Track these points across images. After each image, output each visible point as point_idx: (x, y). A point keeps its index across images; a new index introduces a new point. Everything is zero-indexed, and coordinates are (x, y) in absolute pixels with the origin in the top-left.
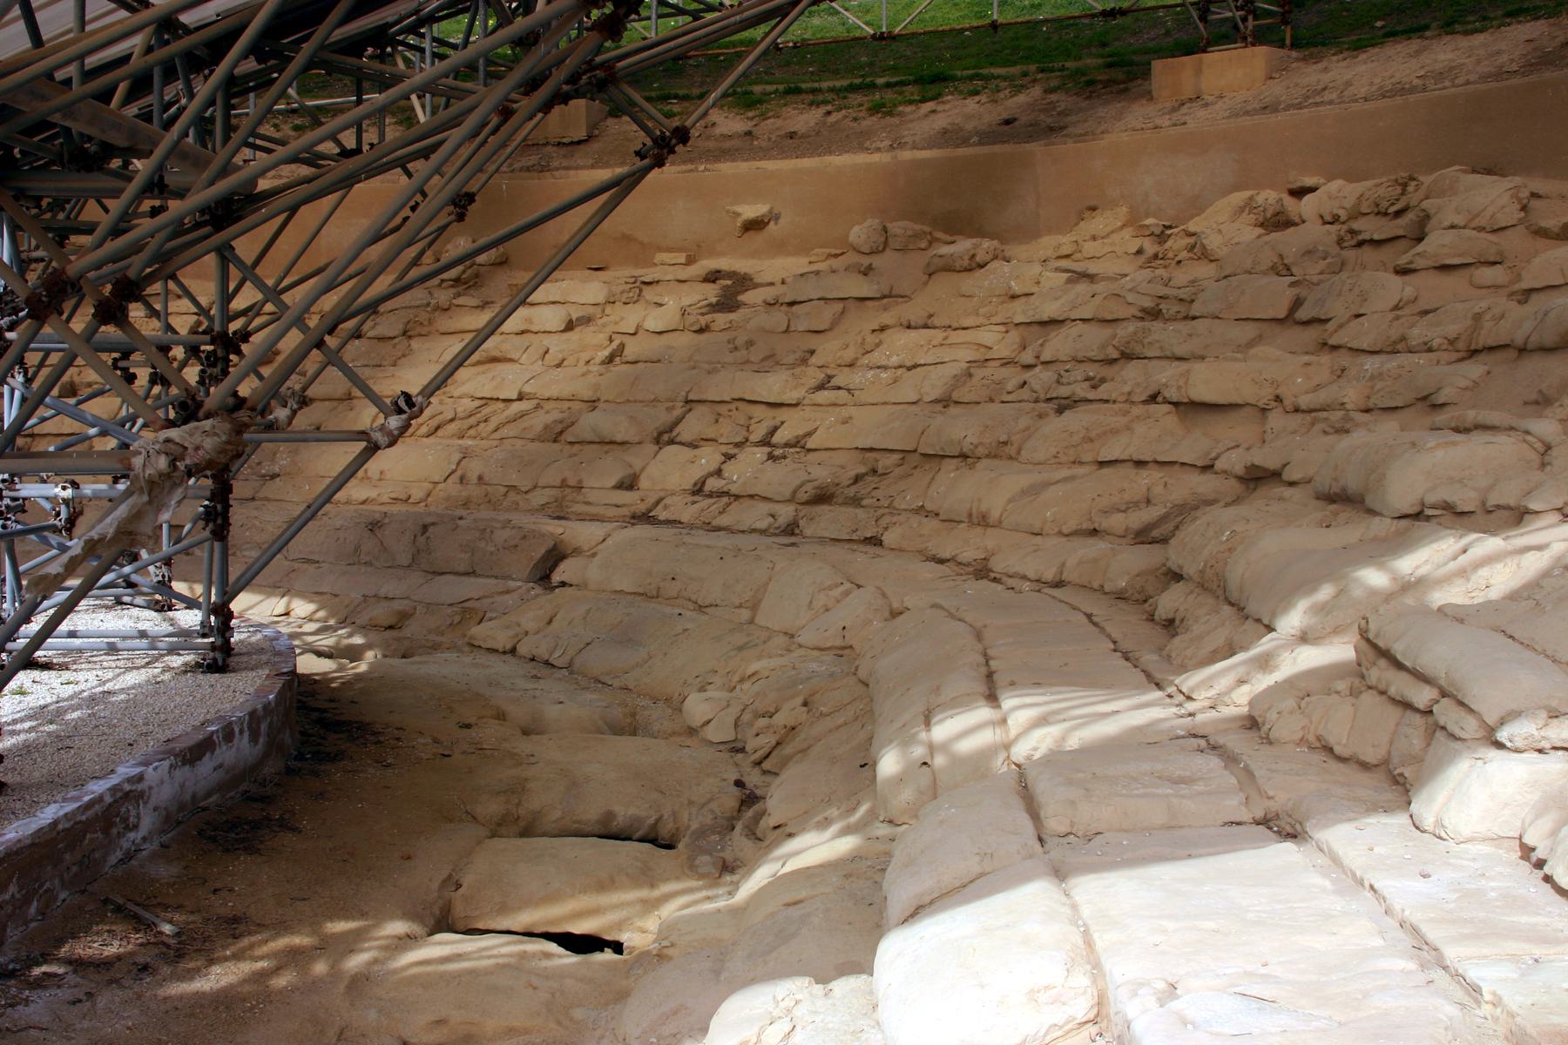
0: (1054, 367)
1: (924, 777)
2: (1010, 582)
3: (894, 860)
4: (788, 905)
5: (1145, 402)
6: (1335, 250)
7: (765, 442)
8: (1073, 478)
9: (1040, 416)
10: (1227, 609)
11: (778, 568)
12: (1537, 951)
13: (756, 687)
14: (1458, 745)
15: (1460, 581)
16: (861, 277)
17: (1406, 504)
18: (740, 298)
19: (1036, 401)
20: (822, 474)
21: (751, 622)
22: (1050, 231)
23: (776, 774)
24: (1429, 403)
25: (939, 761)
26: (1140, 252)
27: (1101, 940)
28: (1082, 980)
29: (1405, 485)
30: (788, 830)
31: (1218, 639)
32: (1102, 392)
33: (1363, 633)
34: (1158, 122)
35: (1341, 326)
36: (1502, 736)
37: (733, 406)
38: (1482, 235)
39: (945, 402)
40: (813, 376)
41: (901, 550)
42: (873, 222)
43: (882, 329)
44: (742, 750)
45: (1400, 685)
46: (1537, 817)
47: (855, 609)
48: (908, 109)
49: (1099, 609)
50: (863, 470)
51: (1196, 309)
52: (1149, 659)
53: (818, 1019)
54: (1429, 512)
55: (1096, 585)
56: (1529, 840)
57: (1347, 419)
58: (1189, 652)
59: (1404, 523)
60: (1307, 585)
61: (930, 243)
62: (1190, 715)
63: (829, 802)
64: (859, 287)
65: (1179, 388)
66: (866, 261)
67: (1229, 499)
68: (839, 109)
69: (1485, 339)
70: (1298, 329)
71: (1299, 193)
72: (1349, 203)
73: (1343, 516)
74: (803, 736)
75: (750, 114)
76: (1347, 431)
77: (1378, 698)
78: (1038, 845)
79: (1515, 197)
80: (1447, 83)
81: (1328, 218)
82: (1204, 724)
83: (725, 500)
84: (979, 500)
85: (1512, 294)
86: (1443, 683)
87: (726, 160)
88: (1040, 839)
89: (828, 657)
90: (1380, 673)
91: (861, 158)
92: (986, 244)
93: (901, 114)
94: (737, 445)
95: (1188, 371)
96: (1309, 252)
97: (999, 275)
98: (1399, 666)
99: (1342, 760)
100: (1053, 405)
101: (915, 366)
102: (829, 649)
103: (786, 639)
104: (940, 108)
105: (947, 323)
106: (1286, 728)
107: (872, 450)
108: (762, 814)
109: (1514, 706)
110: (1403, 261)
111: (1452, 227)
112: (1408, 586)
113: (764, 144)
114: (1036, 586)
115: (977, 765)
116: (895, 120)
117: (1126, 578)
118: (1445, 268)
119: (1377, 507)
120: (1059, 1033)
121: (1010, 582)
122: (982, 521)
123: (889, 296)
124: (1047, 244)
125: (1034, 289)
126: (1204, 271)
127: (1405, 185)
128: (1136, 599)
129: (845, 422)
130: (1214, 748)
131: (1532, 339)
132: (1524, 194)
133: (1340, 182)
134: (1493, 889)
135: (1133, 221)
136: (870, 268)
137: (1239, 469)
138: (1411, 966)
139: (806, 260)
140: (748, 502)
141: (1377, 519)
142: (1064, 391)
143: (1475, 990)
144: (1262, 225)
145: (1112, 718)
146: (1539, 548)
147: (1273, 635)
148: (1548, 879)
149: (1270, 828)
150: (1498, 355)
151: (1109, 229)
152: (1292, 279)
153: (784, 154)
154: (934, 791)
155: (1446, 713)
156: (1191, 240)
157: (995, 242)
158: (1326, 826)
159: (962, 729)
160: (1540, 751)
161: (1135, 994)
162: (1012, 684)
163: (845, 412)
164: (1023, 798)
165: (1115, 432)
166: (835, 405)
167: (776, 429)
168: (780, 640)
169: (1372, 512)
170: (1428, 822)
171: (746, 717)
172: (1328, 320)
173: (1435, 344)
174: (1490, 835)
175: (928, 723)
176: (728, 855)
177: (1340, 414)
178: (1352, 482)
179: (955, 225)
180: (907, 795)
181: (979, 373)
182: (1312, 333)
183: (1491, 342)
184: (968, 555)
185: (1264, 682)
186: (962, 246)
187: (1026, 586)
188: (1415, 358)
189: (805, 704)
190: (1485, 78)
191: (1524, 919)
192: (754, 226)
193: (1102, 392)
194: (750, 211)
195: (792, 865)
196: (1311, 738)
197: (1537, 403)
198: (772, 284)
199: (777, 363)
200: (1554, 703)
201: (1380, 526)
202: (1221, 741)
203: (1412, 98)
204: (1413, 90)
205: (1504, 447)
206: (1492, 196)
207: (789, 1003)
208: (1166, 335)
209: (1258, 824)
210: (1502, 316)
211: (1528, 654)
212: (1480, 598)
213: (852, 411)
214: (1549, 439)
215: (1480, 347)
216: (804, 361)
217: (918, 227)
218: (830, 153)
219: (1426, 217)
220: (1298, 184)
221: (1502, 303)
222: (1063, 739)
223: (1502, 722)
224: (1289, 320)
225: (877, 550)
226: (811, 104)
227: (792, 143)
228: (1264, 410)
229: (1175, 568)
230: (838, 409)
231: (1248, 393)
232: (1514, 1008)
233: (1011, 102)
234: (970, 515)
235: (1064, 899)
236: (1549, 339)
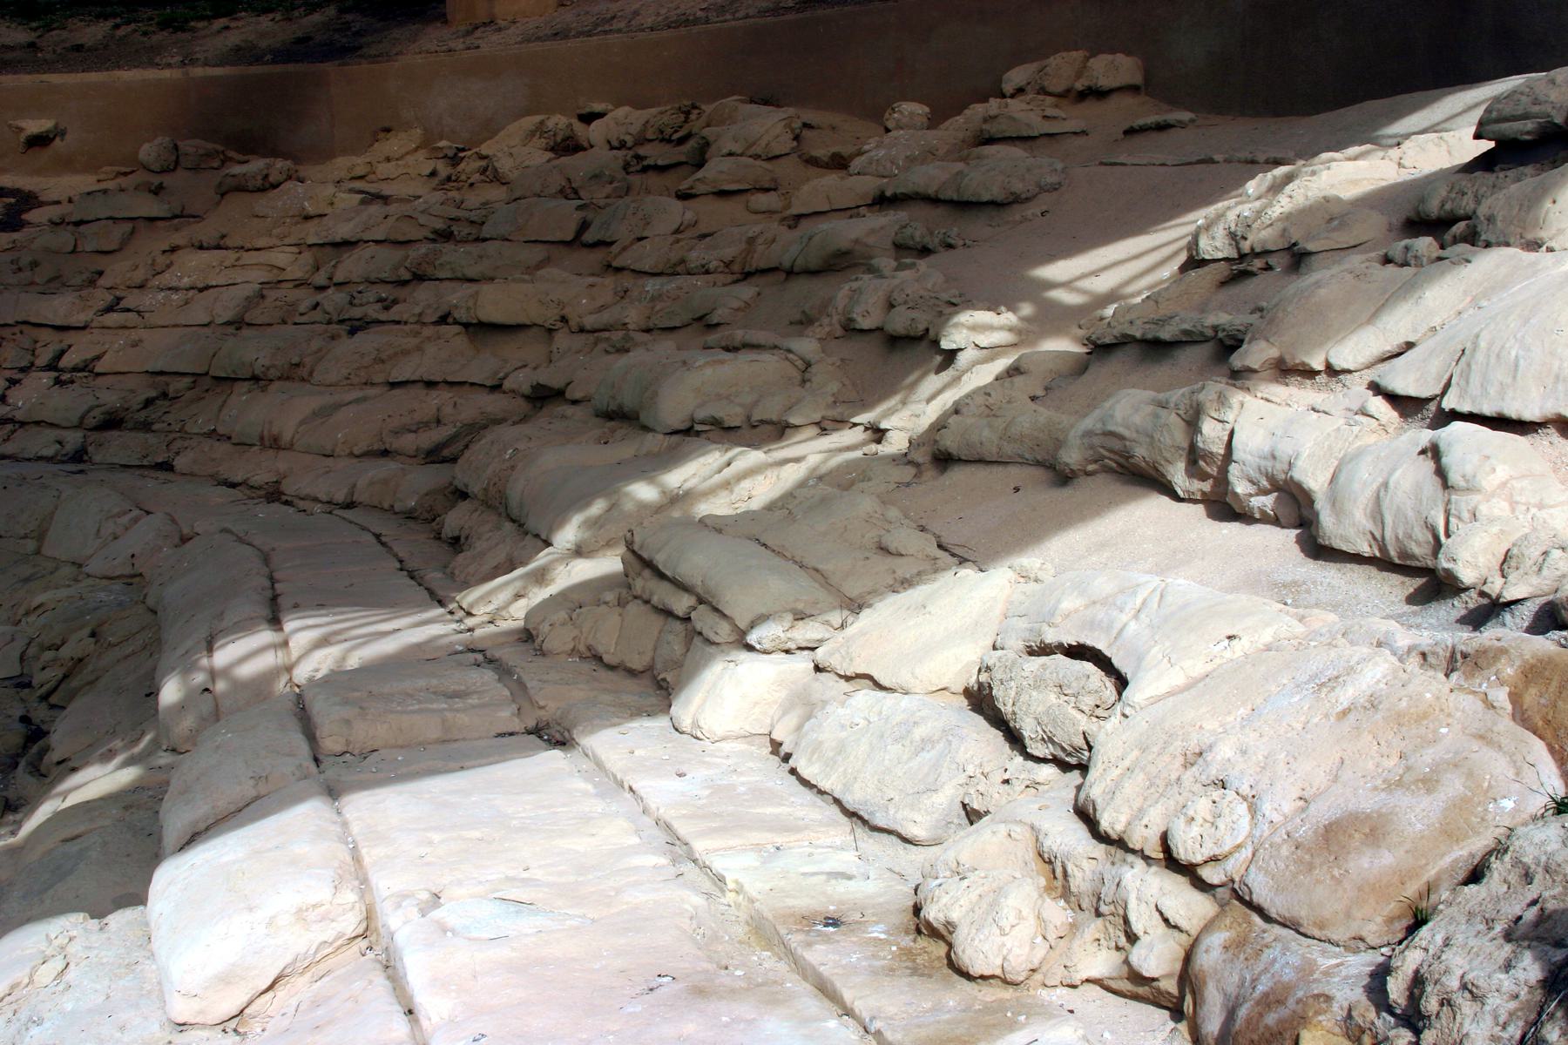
0: (347, 289)
1: (206, 705)
2: (302, 504)
3: (171, 789)
4: (65, 841)
5: (436, 323)
6: (621, 174)
7: (52, 366)
8: (365, 399)
9: (333, 338)
10: (508, 526)
11: (64, 496)
12: (779, 840)
13: (42, 620)
14: (712, 649)
15: (725, 493)
16: (151, 196)
17: (676, 420)
18: (24, 216)
19: (329, 323)
20: (110, 397)
21: (38, 552)
22: (344, 152)
23: (64, 708)
24: (705, 322)
25: (221, 686)
26: (433, 174)
27: (369, 855)
28: (350, 897)
29: (675, 405)
30: (71, 764)
31: (500, 556)
32: (394, 313)
33: (629, 545)
34: (452, 45)
35: (624, 249)
36: (752, 638)
37: (17, 330)
38: (758, 163)
39: (238, 323)
40: (102, 298)
41: (192, 474)
42: (163, 140)
43: (174, 249)
44: (29, 685)
45: (663, 594)
46: (785, 713)
47: (143, 536)
48: (200, 25)
49: (387, 528)
50: (153, 394)
51: (486, 231)
52: (434, 577)
53: (92, 954)
54: (698, 428)
55: (386, 506)
56: (777, 736)
57: (627, 338)
58: (471, 569)
59: (675, 438)
60: (582, 501)
61: (223, 162)
62: (469, 630)
63: (113, 734)
64: (149, 206)
65: (468, 309)
66: (156, 180)
67: (516, 418)
68: (128, 23)
69: (758, 261)
70: (585, 251)
71: (588, 118)
72: (635, 129)
73: (619, 433)
74: (90, 668)
75: (34, 25)
76: (627, 351)
77: (643, 608)
78: (312, 766)
79: (788, 126)
80: (728, 17)
81: (616, 144)
82: (483, 638)
83: (9, 427)
84: (271, 423)
85: (784, 219)
86: (699, 590)
87: (8, 73)
88: (317, 760)
89: (117, 586)
90: (645, 583)
91: (151, 74)
92: (280, 164)
93: (193, 30)
94: (22, 370)
95: (477, 293)
96: (595, 176)
97: (293, 196)
98: (662, 576)
99: (611, 668)
100: (345, 327)
101: (207, 288)
102: (118, 577)
103: (74, 569)
104: (233, 25)
105: (240, 243)
106: (558, 639)
107: (162, 373)
108: (46, 750)
109: (764, 611)
110: (684, 186)
111: (731, 154)
112: (677, 499)
113: (48, 56)
114: (327, 508)
115: (260, 687)
116: (187, 36)
117: (416, 498)
118: (723, 194)
119: (650, 423)
120: (330, 950)
121: (302, 504)
122: (274, 443)
123: (181, 216)
124: (342, 165)
125: (329, 210)
126: (496, 193)
127: (687, 113)
128: (425, 517)
129: (135, 345)
130: (491, 661)
131: (799, 262)
132: (797, 124)
133: (627, 108)
134: (743, 784)
135: (427, 144)
136: (161, 187)
137: (526, 389)
138: (663, 861)
139: (95, 178)
140: (35, 429)
141: (650, 436)
142: (357, 312)
143: (720, 880)
144: (552, 149)
145: (391, 637)
146: (797, 460)
147: (550, 549)
148: (793, 771)
149: (540, 737)
150: (770, 278)
151: (403, 151)
152: (579, 202)
153: (70, 68)
154: (216, 715)
155: (704, 620)
156: (483, 163)
157: (289, 163)
158: (592, 732)
159: (243, 654)
160: (787, 652)
161: (399, 906)
162: (296, 606)
163: (134, 335)
164: (301, 719)
165: (406, 353)
166: (125, 327)
167: (63, 352)
168: (67, 571)
169: (646, 429)
170: (686, 724)
171: (32, 651)
172: (612, 243)
173: (711, 266)
174: (743, 733)
175: (210, 649)
176: (11, 794)
177: (621, 334)
178: (628, 400)
179: (249, 145)
180: (188, 722)
181: (272, 295)
182: (598, 256)
183: (763, 265)
184: (261, 477)
185: (539, 595)
186: (256, 165)
187: (318, 508)
188: (693, 280)
189: (93, 635)
190: (762, 13)
191: (769, 810)
192: (39, 141)
193: (394, 313)
194: (34, 126)
195: (71, 801)
196: (582, 648)
197: (801, 323)
198: (58, 202)
199: (64, 285)
200: (800, 606)
201: (653, 442)
202: (497, 654)
203: (695, 29)
204: (696, 21)
205: (769, 363)
206: (767, 126)
207: (63, 940)
208: (457, 256)
209: (529, 733)
210: (774, 240)
211: (777, 561)
212: (743, 507)
213: (142, 333)
214: (808, 357)
215: (752, 269)
216: (92, 283)
217: (210, 146)
218: (119, 68)
219: (708, 144)
220: (588, 110)
221: (774, 228)
222: (344, 659)
223: (752, 626)
224: (576, 242)
225: (169, 476)
226: (98, 17)
227: (79, 57)
228: (550, 331)
229: (461, 486)
230: (127, 332)
231: (533, 313)
232: (754, 894)
233: (306, 21)
234: (262, 438)
235: (335, 817)
236: (814, 263)
